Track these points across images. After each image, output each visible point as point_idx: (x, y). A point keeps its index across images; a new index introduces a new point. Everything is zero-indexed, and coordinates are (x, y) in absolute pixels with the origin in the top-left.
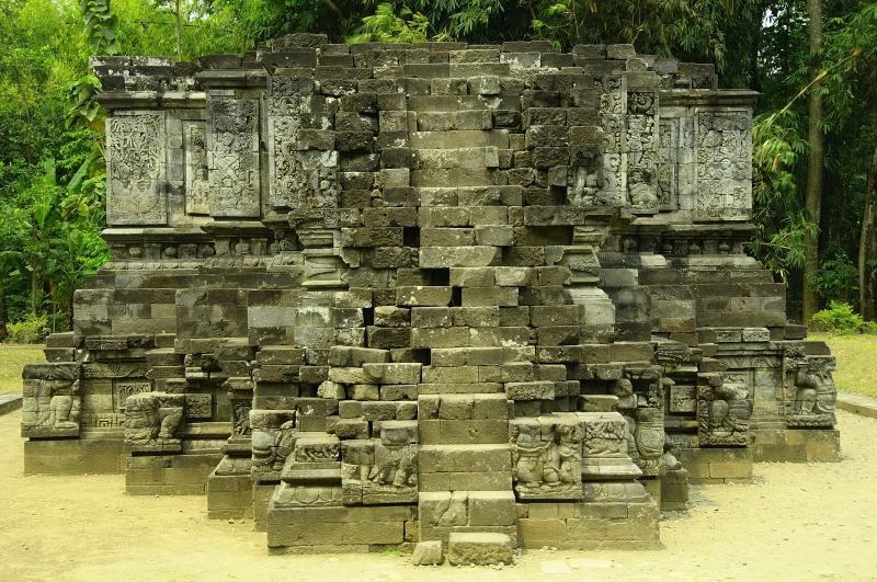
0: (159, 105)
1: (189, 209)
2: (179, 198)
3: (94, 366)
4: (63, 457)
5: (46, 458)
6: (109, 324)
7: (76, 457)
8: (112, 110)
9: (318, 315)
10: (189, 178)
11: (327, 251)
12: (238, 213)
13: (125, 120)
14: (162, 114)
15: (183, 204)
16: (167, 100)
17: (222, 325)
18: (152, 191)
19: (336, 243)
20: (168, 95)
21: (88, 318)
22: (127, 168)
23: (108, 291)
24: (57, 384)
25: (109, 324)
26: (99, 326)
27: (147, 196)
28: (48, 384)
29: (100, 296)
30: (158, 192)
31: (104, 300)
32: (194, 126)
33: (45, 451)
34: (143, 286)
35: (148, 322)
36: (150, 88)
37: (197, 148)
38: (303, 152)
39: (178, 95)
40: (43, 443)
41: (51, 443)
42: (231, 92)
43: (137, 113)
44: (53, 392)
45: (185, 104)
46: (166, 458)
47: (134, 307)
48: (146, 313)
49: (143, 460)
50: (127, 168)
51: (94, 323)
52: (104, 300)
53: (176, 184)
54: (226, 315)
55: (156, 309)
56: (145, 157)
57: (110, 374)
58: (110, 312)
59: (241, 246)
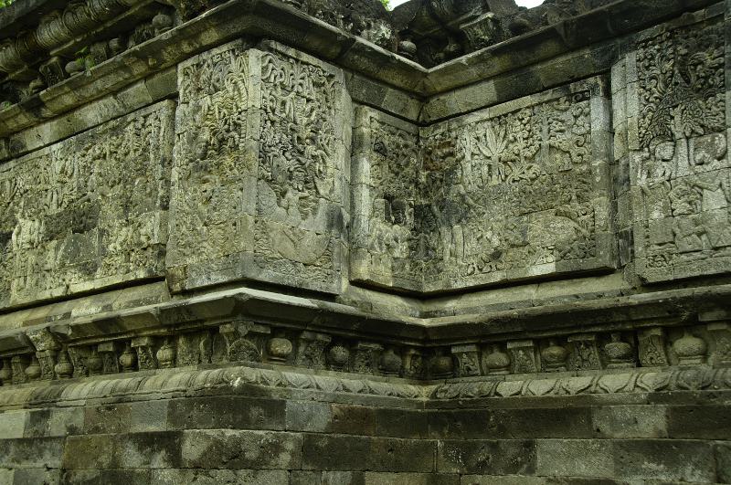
1: (363, 270)
22: (287, 163)
29: (277, 448)
30: (330, 226)
31: (285, 458)
32: (375, 114)
43: (305, 57)
52: (285, 458)
53: (347, 217)
56: (311, 149)
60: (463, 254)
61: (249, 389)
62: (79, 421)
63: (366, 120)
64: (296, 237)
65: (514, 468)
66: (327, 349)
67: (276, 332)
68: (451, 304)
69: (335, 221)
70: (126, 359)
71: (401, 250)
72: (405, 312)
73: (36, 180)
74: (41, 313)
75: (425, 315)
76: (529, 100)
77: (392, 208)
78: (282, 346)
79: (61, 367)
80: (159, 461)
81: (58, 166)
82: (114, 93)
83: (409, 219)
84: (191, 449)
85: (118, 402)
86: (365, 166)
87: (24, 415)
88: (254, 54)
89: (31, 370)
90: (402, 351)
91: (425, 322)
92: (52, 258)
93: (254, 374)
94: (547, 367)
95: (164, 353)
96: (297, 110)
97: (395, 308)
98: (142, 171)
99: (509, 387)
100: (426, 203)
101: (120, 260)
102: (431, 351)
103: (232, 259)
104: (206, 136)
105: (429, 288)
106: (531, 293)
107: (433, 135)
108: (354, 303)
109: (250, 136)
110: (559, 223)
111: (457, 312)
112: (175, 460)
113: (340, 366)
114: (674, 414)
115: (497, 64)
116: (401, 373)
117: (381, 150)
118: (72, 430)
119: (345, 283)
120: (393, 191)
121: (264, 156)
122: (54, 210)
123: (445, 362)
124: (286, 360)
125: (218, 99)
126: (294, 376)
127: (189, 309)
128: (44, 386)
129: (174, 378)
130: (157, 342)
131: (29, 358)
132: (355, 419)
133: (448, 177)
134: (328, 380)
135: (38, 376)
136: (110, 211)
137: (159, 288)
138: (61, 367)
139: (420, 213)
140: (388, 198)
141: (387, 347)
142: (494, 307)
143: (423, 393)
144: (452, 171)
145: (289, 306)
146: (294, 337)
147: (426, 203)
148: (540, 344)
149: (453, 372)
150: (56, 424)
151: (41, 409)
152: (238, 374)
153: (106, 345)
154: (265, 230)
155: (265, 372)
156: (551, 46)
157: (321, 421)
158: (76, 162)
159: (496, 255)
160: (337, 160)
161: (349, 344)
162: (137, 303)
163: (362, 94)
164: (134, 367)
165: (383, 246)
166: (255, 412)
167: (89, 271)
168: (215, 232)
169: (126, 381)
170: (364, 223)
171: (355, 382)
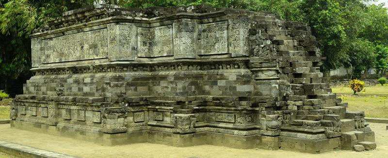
0: (132, 21)
1: (139, 55)
2: (136, 52)
3: (128, 108)
4: (123, 139)
5: (118, 140)
6: (125, 94)
7: (126, 138)
8: (118, 22)
9: (276, 87)
10: (139, 45)
11: (275, 68)
12: (191, 57)
13: (123, 26)
14: (133, 24)
15: (137, 54)
16: (136, 20)
17: (194, 92)
18: (130, 49)
19: (278, 66)
20: (136, 18)
21: (119, 92)
22: (124, 41)
23: (125, 83)
24: (120, 114)
25: (125, 94)
26: (122, 94)
27: (129, 51)
28: (118, 115)
29: (123, 84)
30: (132, 50)
31: (124, 85)
32: (140, 28)
33: (117, 137)
34: (132, 81)
35: (136, 93)
36: (130, 16)
37: (141, 36)
38: (264, 40)
39: (139, 19)
40: (117, 135)
41: (119, 134)
42: (189, 20)
43: (126, 23)
44: (119, 117)
45: (140, 22)
46: (192, 134)
47: (133, 88)
48: (136, 90)
49: (187, 135)
50: (124, 41)
51: (121, 93)
52: (124, 85)
53: (136, 47)
54: (195, 89)
55: (139, 88)
56: (128, 38)
57: (133, 110)
58: (126, 90)
59: (190, 67)
60: (156, 50)
61: (119, 76)
62: (98, 80)
63: (138, 30)
64: (126, 53)
65: (158, 85)
66: (133, 69)
67: (124, 67)
68: (155, 59)
69: (134, 49)
70: (104, 70)
71: (147, 51)
72: (147, 61)
73: (87, 37)
74: (90, 61)
75: (151, 61)
76: (163, 27)
77: (145, 43)
78: (125, 69)
79: (94, 71)
80: (108, 86)
81: (90, 36)
82: (98, 25)
83: (148, 45)
84: (112, 85)
85: (103, 77)
86: (139, 38)
87: (90, 79)
88: (118, 26)
89: (90, 71)
90: (147, 67)
91: (150, 63)
92: (91, 52)
93: (120, 74)
94: (166, 70)
95: (109, 70)
96: (126, 33)
97: (146, 61)
98: (104, 40)
99: (160, 73)
100: (150, 42)
101: (101, 54)
102: (152, 67)
103: (117, 57)
104: (112, 37)
105: (152, 56)
106: (164, 58)
107: (152, 30)
108: (137, 61)
109: (118, 38)
110: (167, 48)
111: (156, 61)
112: (110, 86)
113: (135, 71)
114: (175, 77)
115: (159, 21)
116: (147, 71)
117: (142, 34)
118: (97, 82)
119: (136, 58)
120: (144, 41)
121: (120, 41)
122: (90, 44)
123: (154, 69)
124: (126, 71)
125: (113, 31)
126: (126, 73)
127: (111, 65)
128: (92, 74)
129: (110, 74)
130: (108, 68)
131: (89, 69)
132: (136, 79)
133: (153, 38)
134: (132, 73)
135: (91, 72)
136: (99, 45)
137: (107, 59)
138: (94, 71)
139: (150, 43)
140: (144, 42)
141: (144, 67)
142: (161, 60)
143: (150, 74)
144: (154, 37)
145: (125, 64)
146: (127, 67)
147: (150, 42)
148: (165, 67)
149: (155, 70)
150: (95, 81)
151: (92, 77)
152: (118, 74)
153: (100, 68)
154: (121, 52)
155: (122, 73)
156: (165, 20)
157: (131, 79)
158: (93, 36)
159: (160, 52)
160: (133, 38)
161: (136, 67)
162: (104, 62)
163: (138, 25)
164: (105, 72)
165: (143, 50)
166: (120, 80)
167: (97, 55)
168: (114, 53)
169: (104, 74)
170: (139, 47)
171: (137, 73)
